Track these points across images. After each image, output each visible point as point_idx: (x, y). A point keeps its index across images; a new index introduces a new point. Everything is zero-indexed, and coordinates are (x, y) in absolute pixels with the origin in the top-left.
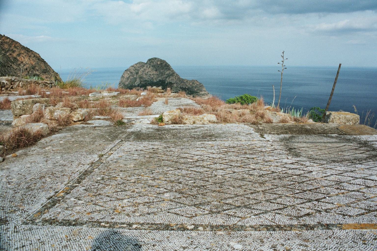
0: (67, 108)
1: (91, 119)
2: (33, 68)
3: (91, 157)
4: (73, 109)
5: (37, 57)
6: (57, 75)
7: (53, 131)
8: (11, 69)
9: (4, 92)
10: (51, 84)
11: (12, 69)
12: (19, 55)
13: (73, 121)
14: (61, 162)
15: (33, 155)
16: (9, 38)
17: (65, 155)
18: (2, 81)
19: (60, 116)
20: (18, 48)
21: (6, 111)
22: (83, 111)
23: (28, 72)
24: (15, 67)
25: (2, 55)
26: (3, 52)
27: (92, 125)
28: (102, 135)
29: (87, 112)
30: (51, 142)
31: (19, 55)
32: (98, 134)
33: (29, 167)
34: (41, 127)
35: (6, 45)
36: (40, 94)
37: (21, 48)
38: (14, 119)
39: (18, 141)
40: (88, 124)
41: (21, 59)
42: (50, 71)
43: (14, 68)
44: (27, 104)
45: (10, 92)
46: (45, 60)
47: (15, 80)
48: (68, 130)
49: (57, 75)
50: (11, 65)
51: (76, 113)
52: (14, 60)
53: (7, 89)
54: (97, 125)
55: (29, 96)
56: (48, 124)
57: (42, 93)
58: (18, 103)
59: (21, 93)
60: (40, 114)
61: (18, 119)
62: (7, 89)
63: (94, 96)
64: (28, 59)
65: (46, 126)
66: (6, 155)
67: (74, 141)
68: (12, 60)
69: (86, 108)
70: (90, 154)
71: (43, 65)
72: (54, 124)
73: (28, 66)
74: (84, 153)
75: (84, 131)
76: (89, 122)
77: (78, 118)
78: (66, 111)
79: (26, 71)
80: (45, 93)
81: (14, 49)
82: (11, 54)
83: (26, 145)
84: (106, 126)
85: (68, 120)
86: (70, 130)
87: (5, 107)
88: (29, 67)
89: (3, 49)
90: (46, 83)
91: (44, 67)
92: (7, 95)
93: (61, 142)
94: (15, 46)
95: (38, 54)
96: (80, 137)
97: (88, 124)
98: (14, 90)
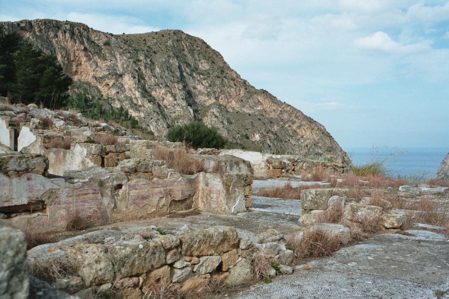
0: (377, 207)
1: (412, 228)
2: (314, 145)
3: (422, 293)
4: (385, 209)
5: (321, 130)
6: (345, 156)
7: (355, 240)
8: (288, 145)
9: (284, 174)
10: (343, 167)
11: (290, 144)
12: (299, 127)
13: (384, 226)
14: (374, 291)
15: (331, 271)
16: (290, 105)
17: (379, 281)
18: (283, 161)
19: (365, 217)
20: (299, 118)
21: (288, 201)
22: (401, 214)
23: (309, 150)
24: (293, 142)
25: (280, 126)
26: (281, 123)
27: (413, 238)
28: (433, 256)
29: (407, 216)
30: (355, 256)
31: (299, 127)
32: (427, 253)
33: (328, 290)
34: (341, 230)
35: (285, 114)
36: (329, 181)
37: (303, 119)
38: (303, 215)
39: (312, 247)
40: (408, 234)
41: (302, 133)
42: (336, 149)
43: (291, 144)
44: (321, 195)
45: (290, 175)
46: (331, 135)
47: (299, 160)
48: (378, 240)
49: (345, 156)
50: (289, 140)
51: (389, 215)
52: (293, 133)
53: (287, 171)
54: (422, 238)
55: (315, 183)
56: (349, 227)
57: (332, 179)
58: (310, 193)
59: (305, 178)
60: (337, 211)
61: (306, 215)
62: (287, 171)
63: (406, 191)
64: (310, 132)
65: (347, 229)
66: (296, 265)
67: (388, 260)
68: (291, 134)
69: (398, 208)
70: (420, 286)
71: (327, 141)
72: (357, 229)
73: (309, 141)
74: (409, 283)
75: (403, 245)
76: (410, 231)
77: (393, 224)
78: (376, 210)
79: (306, 148)
80: (335, 181)
81: (295, 120)
82: (290, 126)
83: (321, 255)
84: (438, 242)
85: (377, 224)
86: (380, 241)
87: (287, 195)
88: (310, 143)
89: (282, 120)
90: (336, 166)
91: (329, 143)
92: (288, 179)
93: (369, 258)
94: (296, 115)
95: (323, 126)
96: (397, 255)
97: (408, 234)
98: (295, 173)
